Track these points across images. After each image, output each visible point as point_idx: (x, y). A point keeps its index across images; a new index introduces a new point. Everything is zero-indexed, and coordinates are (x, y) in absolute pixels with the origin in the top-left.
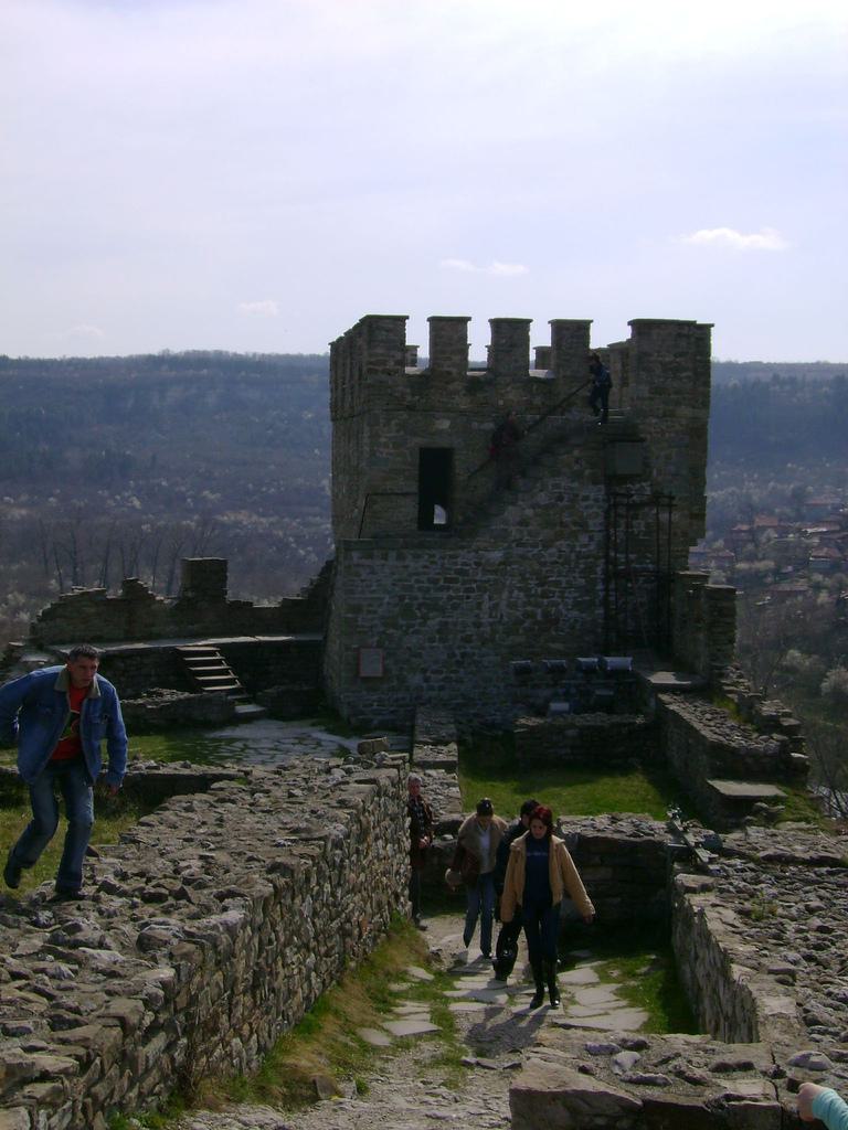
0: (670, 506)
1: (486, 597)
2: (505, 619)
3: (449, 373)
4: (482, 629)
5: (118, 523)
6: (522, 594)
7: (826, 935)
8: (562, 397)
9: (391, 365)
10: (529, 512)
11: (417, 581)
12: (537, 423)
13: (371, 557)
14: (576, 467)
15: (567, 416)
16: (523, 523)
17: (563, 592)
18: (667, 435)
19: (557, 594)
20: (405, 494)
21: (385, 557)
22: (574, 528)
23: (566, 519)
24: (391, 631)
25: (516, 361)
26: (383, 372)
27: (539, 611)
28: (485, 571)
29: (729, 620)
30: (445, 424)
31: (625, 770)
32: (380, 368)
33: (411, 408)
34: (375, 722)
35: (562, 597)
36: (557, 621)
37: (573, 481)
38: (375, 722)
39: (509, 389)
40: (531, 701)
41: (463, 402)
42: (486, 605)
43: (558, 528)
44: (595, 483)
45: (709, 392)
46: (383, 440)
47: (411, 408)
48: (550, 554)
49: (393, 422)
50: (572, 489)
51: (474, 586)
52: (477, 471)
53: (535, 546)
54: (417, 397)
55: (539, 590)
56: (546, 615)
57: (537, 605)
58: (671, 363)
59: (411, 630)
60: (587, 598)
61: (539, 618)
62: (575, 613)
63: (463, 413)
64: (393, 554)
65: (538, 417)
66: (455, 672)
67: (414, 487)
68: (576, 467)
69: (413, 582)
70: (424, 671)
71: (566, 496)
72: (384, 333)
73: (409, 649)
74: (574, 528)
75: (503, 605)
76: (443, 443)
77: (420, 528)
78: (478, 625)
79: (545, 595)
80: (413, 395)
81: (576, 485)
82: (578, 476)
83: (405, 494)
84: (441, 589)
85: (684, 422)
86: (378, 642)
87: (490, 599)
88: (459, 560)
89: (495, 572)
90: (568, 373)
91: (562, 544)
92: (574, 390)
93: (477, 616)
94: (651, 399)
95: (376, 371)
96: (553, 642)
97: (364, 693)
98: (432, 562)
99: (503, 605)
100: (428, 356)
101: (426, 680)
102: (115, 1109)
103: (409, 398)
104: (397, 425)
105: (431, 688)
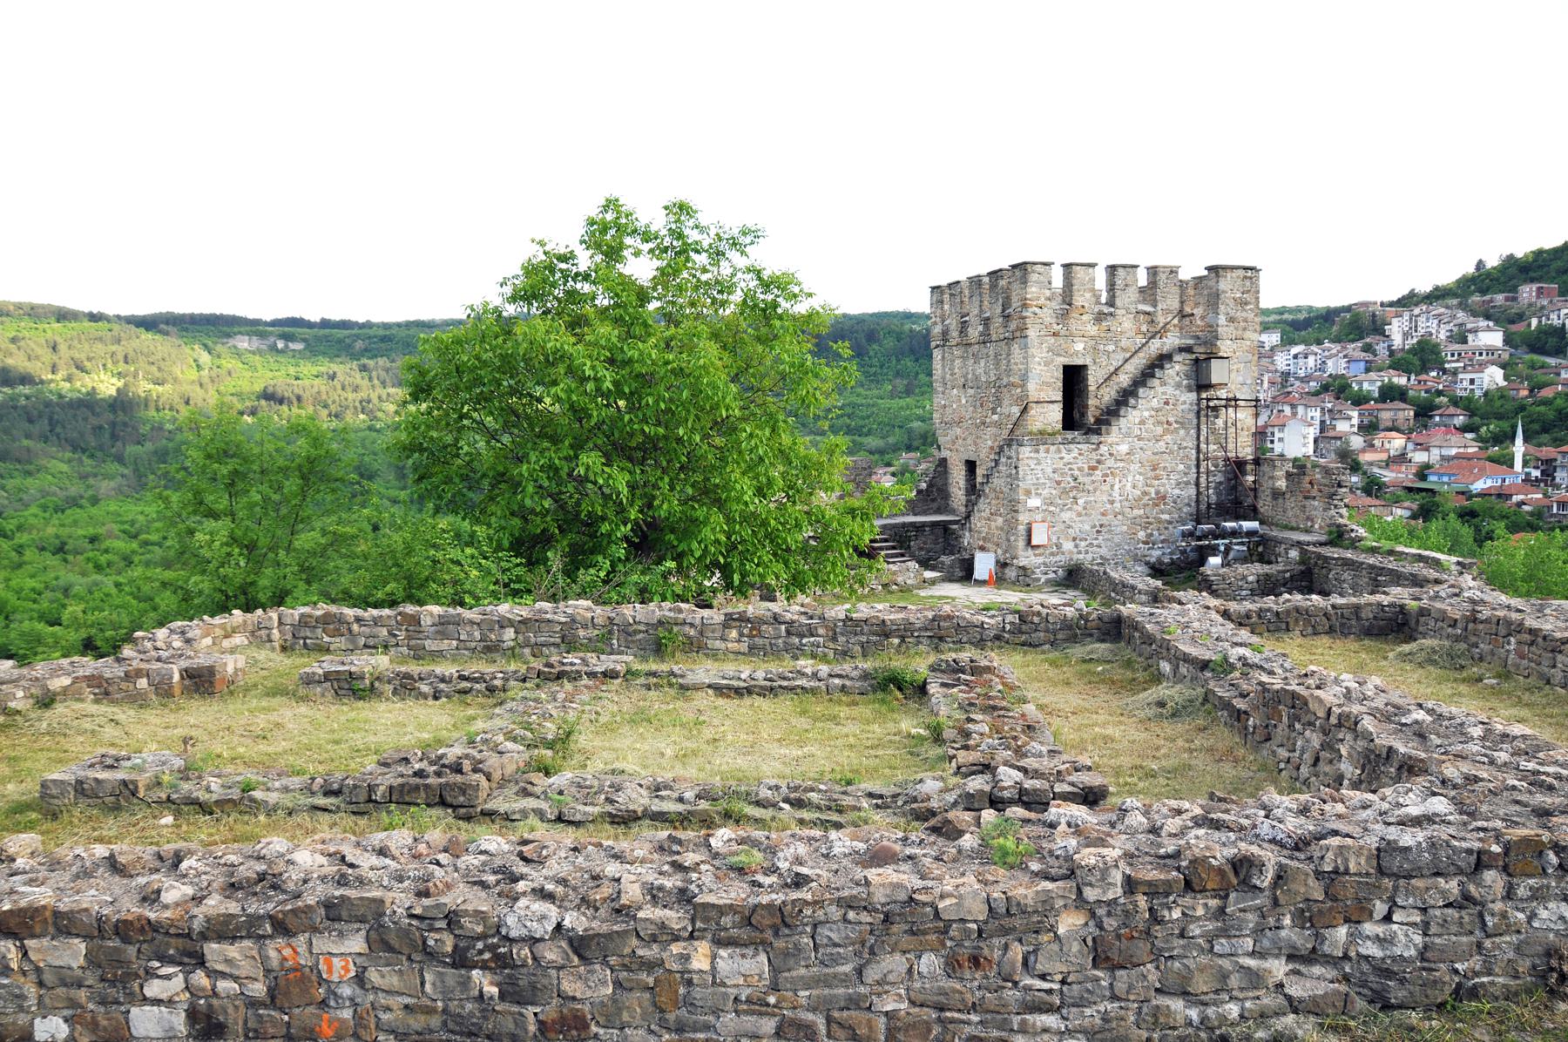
0: (1236, 406)
7: (785, 666)
10: (1146, 414)
13: (1037, 451)
21: (1047, 451)
23: (1171, 419)
27: (1153, 491)
30: (1079, 346)
36: (1164, 498)
41: (1093, 330)
42: (1116, 487)
44: (1190, 391)
48: (1161, 446)
56: (1157, 493)
62: (1177, 491)
64: (1053, 448)
67: (1059, 396)
70: (1074, 539)
76: (1079, 362)
77: (1064, 428)
82: (1178, 386)
86: (1244, 473)
88: (76, 744)
91: (1168, 438)
100: (1061, 285)
102: (1562, 977)
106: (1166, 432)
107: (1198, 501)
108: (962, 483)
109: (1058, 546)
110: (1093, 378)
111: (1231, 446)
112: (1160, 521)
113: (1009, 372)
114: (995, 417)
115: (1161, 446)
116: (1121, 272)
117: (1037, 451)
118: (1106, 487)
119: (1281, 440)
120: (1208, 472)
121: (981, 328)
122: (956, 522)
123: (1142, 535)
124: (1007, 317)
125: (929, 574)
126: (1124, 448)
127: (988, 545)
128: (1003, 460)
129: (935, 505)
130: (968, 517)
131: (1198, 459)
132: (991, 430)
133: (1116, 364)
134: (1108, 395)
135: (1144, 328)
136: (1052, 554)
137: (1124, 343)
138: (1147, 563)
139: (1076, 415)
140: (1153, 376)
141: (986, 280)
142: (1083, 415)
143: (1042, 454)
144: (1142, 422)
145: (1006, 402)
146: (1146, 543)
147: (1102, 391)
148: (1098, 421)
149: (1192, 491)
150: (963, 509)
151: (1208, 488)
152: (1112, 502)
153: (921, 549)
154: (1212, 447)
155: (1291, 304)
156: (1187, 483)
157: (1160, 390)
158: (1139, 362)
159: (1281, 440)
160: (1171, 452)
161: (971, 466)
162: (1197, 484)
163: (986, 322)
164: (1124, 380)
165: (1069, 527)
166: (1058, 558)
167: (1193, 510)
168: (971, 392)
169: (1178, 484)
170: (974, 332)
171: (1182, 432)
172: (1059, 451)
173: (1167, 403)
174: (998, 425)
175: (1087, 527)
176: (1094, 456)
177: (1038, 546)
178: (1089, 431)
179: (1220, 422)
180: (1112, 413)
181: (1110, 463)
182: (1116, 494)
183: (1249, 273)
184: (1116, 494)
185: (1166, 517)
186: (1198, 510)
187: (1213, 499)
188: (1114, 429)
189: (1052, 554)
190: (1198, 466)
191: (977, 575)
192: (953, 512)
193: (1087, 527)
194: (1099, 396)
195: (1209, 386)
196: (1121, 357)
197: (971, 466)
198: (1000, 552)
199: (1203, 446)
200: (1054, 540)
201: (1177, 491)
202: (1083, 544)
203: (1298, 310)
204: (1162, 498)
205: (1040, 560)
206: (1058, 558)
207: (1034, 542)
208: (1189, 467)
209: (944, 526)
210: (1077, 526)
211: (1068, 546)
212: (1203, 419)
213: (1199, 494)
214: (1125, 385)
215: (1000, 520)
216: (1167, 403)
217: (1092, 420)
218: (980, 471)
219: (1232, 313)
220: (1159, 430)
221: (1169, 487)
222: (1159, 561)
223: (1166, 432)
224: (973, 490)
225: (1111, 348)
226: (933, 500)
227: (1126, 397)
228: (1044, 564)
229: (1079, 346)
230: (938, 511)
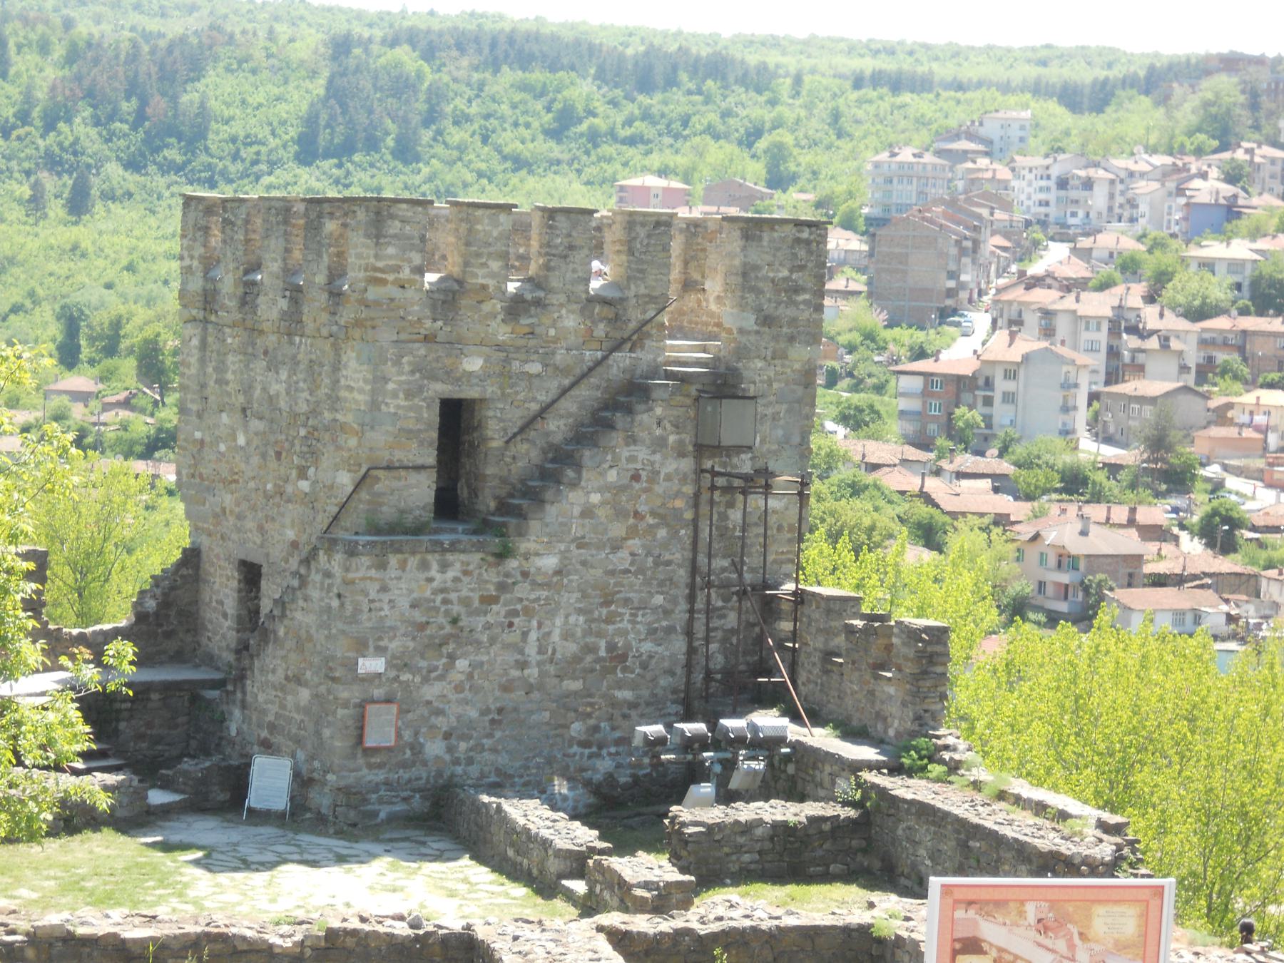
1: (535, 623)
2: (558, 656)
3: (484, 287)
4: (526, 672)
5: (666, 821)
6: (581, 619)
8: (633, 325)
9: (406, 273)
11: (445, 601)
12: (598, 363)
14: (658, 432)
15: (639, 354)
16: (587, 512)
17: (635, 615)
18: (775, 385)
19: (627, 617)
20: (419, 468)
22: (651, 521)
23: (642, 508)
24: (406, 677)
25: (574, 271)
26: (395, 282)
27: (603, 644)
28: (535, 584)
29: (939, 669)
31: (659, 851)
32: (391, 277)
33: (428, 339)
34: (382, 815)
35: (633, 622)
36: (623, 658)
37: (654, 452)
38: (382, 815)
39: (564, 311)
40: (588, 774)
41: (503, 333)
42: (533, 636)
43: (631, 521)
44: (682, 455)
45: (822, 320)
46: (391, 386)
47: (428, 339)
49: (405, 360)
50: (652, 463)
51: (519, 607)
52: (515, 435)
53: (600, 547)
54: (440, 323)
55: (604, 611)
56: (611, 647)
57: (599, 634)
58: (785, 279)
59: (594, 749)
60: (664, 623)
61: (602, 653)
62: (647, 647)
63: (499, 347)
65: (599, 354)
66: (490, 736)
67: (430, 457)
68: (658, 432)
69: (438, 603)
70: (447, 736)
71: (643, 474)
72: (397, 223)
73: (429, 703)
74: (651, 521)
75: (556, 637)
76: (469, 392)
78: (523, 665)
79: (609, 621)
80: (435, 320)
81: (657, 457)
82: (660, 444)
83: (419, 468)
84: (477, 613)
85: (797, 366)
87: (540, 625)
89: (547, 585)
90: (642, 291)
91: (635, 544)
92: (651, 313)
93: (522, 652)
94: (758, 332)
95: (383, 282)
96: (620, 688)
97: (365, 771)
98: (466, 573)
99: (556, 637)
101: (450, 749)
103: (428, 323)
104: (409, 363)
105: (456, 762)
106: (632, 532)
107: (689, 666)
108: (231, 604)
109: (416, 748)
110: (495, 427)
111: (753, 560)
112: (614, 704)
113: (334, 401)
114: (304, 485)
115: (622, 559)
116: (562, 223)
117: (383, 566)
118: (513, 637)
119: (1009, 398)
120: (709, 611)
121: (283, 304)
122: (215, 684)
123: (577, 728)
124: (336, 295)
125: (157, 797)
126: (549, 562)
127: (277, 739)
128: (316, 577)
129: (172, 646)
130: (241, 678)
131: (692, 586)
132: (293, 511)
133: (543, 397)
134: (527, 454)
135: (601, 330)
136: (404, 765)
137: (560, 357)
138: (587, 783)
139: (463, 492)
140: (611, 426)
141: (301, 207)
142: (474, 493)
143: (392, 572)
144: (587, 512)
145: (325, 462)
146: (585, 744)
147: (513, 450)
148: (504, 508)
149: (679, 645)
150: (229, 657)
151: (708, 640)
152: (523, 665)
153: (140, 737)
154: (719, 563)
155: (1065, 40)
156: (670, 630)
157: (625, 453)
158: (587, 393)
159: (1009, 398)
160: (641, 571)
161: (251, 574)
162: (689, 633)
163: (295, 294)
164: (557, 427)
165: (439, 712)
166: (414, 772)
167: (680, 683)
168: (256, 425)
169: (652, 632)
170: (271, 308)
171: (662, 533)
172: (424, 566)
173: (636, 477)
174: (310, 500)
175: (474, 714)
176: (492, 576)
177: (375, 750)
178: (485, 527)
179: (736, 516)
180: (527, 496)
181: (522, 591)
182: (531, 650)
183: (805, 234)
184: (531, 650)
185: (625, 694)
186: (688, 683)
187: (718, 661)
188: (534, 525)
189: (404, 765)
190: (691, 598)
191: (255, 799)
192: (210, 660)
193: (474, 714)
194: (503, 456)
195: (718, 449)
196: (554, 385)
197: (251, 574)
198: (301, 755)
199: (702, 559)
200: (407, 735)
201: (647, 647)
202: (463, 746)
203: (1085, 55)
204: (618, 657)
205: (380, 776)
206: (414, 772)
207: (370, 742)
208: (674, 601)
209: (192, 691)
210: (454, 710)
211: (434, 748)
212: (704, 509)
213: (691, 651)
214: (558, 438)
215: (305, 695)
216: (636, 477)
217: (493, 505)
218: (270, 590)
219: (769, 308)
220: (618, 530)
221: (630, 630)
222: (610, 777)
223: (632, 532)
224: (252, 620)
225: (535, 368)
226: (169, 635)
227: (559, 465)
228: (387, 783)
229: (474, 364)
230: (179, 658)
